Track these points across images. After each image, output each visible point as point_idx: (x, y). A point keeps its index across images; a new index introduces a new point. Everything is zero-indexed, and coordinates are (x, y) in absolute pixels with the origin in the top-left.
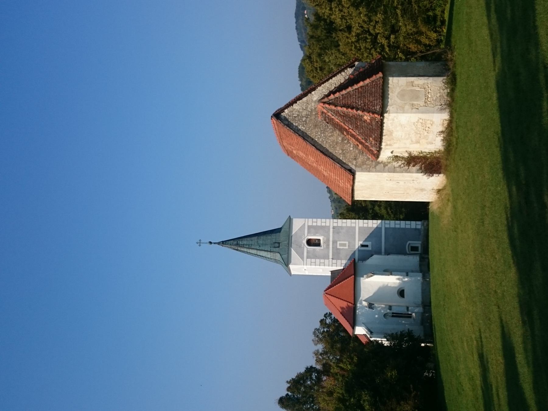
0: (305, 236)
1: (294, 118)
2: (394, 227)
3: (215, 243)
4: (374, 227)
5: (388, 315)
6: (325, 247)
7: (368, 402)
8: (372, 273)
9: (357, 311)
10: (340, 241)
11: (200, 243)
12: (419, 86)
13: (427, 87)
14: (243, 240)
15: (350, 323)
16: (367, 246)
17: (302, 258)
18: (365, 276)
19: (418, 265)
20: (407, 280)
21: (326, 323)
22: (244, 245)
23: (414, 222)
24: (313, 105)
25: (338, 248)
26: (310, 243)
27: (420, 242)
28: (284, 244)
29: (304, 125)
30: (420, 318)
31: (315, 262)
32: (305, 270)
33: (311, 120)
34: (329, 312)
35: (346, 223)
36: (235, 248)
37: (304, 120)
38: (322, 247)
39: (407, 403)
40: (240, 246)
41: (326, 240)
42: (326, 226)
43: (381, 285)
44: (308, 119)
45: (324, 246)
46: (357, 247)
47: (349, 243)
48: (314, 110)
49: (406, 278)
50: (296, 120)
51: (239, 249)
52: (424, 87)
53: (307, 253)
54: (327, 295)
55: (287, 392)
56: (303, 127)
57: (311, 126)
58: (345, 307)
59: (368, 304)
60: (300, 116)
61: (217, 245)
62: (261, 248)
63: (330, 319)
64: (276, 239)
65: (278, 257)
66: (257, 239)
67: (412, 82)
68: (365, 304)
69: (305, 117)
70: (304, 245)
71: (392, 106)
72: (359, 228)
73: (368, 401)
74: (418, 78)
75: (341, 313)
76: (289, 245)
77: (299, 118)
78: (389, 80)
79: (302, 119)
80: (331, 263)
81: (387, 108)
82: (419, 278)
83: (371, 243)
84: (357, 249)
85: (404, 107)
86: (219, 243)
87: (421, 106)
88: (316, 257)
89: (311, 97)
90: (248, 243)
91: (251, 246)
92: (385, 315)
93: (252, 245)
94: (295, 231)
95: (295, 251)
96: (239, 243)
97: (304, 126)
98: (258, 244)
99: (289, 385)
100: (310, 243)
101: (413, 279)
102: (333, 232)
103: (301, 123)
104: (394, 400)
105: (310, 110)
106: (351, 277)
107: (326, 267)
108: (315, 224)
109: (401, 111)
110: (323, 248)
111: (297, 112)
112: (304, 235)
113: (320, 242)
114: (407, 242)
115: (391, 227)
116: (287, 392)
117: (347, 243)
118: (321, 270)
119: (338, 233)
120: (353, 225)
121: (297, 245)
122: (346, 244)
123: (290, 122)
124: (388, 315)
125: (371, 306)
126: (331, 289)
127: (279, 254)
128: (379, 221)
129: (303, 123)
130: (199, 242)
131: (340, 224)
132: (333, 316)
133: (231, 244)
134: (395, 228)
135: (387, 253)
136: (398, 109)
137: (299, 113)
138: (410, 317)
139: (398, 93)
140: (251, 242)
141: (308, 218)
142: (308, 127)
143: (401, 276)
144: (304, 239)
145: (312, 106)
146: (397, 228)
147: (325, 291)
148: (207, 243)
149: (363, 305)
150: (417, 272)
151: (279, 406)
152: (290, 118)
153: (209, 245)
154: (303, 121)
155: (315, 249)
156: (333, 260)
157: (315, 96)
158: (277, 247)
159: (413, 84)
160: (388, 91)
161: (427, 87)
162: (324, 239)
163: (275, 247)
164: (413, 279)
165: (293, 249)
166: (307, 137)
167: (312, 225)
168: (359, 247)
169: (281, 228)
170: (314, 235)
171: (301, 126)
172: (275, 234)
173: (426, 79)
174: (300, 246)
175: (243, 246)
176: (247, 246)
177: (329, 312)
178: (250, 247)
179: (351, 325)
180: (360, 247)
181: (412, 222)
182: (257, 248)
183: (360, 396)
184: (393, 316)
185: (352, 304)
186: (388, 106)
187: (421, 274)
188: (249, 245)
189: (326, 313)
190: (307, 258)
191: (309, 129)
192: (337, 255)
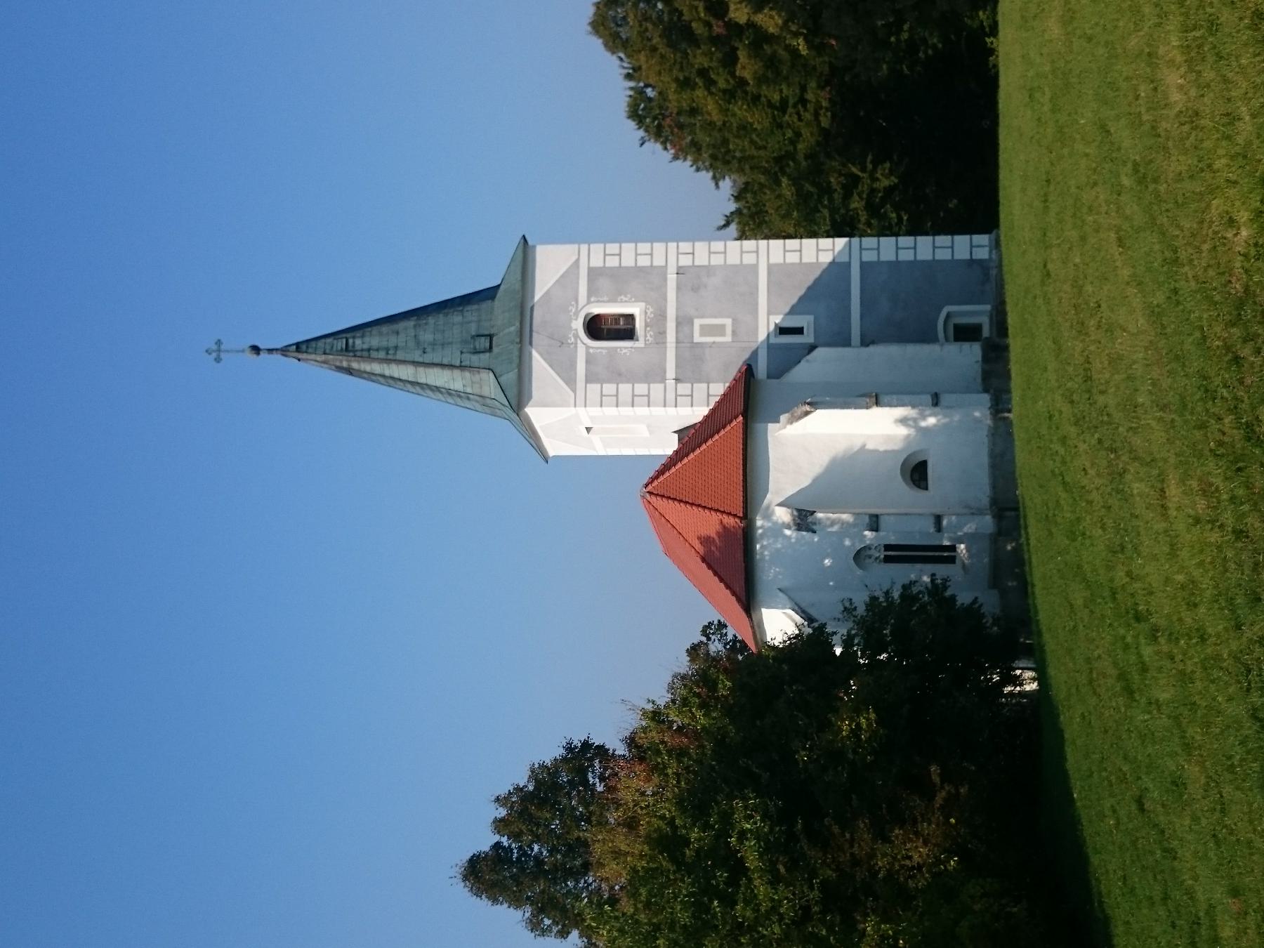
0: (580, 307)
2: (893, 258)
3: (270, 351)
4: (821, 263)
5: (870, 557)
6: (650, 339)
7: (758, 839)
8: (808, 404)
9: (758, 546)
10: (702, 317)
14: (368, 334)
15: (734, 593)
16: (799, 331)
17: (570, 381)
18: (784, 418)
19: (979, 380)
20: (935, 425)
21: (708, 654)
22: (369, 350)
25: (695, 341)
26: (597, 328)
27: (988, 307)
28: (505, 329)
30: (986, 560)
31: (617, 396)
32: (588, 429)
34: (719, 621)
35: (725, 253)
36: (341, 361)
38: (641, 339)
39: (917, 834)
41: (652, 315)
43: (840, 448)
45: (646, 336)
46: (762, 336)
49: (930, 415)
51: (355, 365)
53: (588, 362)
54: (653, 499)
55: (497, 838)
58: (714, 535)
59: (795, 513)
61: (277, 357)
62: (428, 358)
63: (719, 640)
64: (479, 321)
65: (488, 384)
66: (415, 326)
68: (783, 515)
70: (576, 336)
72: (770, 268)
73: (758, 835)
75: (703, 560)
76: (523, 337)
80: (671, 396)
82: (977, 414)
83: (811, 318)
84: (762, 342)
86: (284, 351)
88: (618, 376)
90: (384, 344)
91: (395, 354)
92: (860, 556)
93: (396, 348)
94: (545, 289)
95: (545, 359)
96: (353, 346)
98: (418, 343)
99: (502, 812)
100: (597, 328)
101: (957, 418)
102: (679, 288)
104: (862, 826)
106: (734, 423)
107: (658, 411)
108: (612, 262)
110: (643, 345)
112: (577, 302)
115: (883, 258)
116: (497, 838)
117: (728, 322)
118: (643, 431)
119: (695, 289)
120: (749, 259)
121: (551, 337)
122: (723, 327)
124: (870, 557)
125: (804, 520)
126: (667, 474)
127: (491, 375)
128: (841, 242)
130: (215, 347)
131: (702, 260)
132: (730, 632)
133: (328, 351)
135: (865, 343)
138: (952, 560)
140: (393, 341)
141: (589, 242)
143: (914, 407)
144: (577, 314)
146: (904, 262)
147: (646, 486)
148: (243, 351)
149: (775, 523)
150: (968, 390)
151: (467, 889)
153: (252, 357)
155: (617, 348)
156: (679, 385)
162: (646, 313)
163: (476, 352)
164: (957, 418)
165: (541, 354)
169: (499, 286)
170: (610, 301)
172: (475, 307)
175: (367, 355)
176: (382, 355)
177: (719, 621)
178: (390, 357)
179: (739, 600)
180: (776, 336)
181: (957, 238)
182: (416, 360)
183: (726, 818)
184: (888, 560)
185: (739, 517)
187: (986, 398)
188: (387, 350)
189: (710, 623)
192: (691, 368)
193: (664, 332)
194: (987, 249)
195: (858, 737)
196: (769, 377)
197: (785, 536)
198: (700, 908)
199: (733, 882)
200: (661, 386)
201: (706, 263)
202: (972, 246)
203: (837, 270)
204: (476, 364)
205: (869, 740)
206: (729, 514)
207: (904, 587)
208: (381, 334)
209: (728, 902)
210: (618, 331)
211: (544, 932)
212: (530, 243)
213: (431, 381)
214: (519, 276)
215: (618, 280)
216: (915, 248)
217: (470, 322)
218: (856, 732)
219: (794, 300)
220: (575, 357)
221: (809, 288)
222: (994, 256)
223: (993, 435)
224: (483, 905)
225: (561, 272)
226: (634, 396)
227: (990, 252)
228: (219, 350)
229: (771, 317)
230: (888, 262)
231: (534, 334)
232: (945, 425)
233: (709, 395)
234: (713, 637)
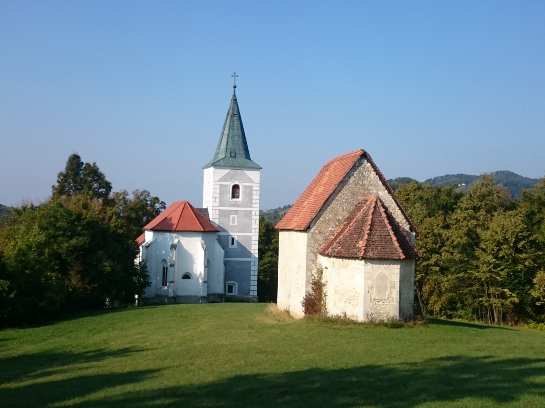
0: (242, 183)
1: (362, 172)
3: (235, 91)
5: (165, 263)
8: (206, 249)
9: (168, 234)
10: (237, 217)
12: (391, 294)
13: (389, 301)
15: (156, 226)
16: (233, 244)
17: (220, 180)
20: (199, 282)
22: (233, 121)
24: (374, 191)
26: (236, 188)
27: (237, 295)
29: (354, 183)
30: (163, 294)
38: (232, 200)
42: (252, 204)
43: (195, 257)
44: (360, 186)
46: (231, 234)
47: (236, 226)
50: (359, 174)
51: (229, 117)
53: (226, 185)
54: (183, 204)
56: (352, 181)
61: (233, 93)
62: (230, 139)
64: (240, 154)
65: (222, 156)
66: (239, 135)
67: (394, 287)
68: (176, 241)
69: (362, 183)
70: (233, 182)
72: (251, 236)
75: (166, 218)
77: (361, 178)
78: (397, 264)
79: (360, 180)
81: (369, 263)
83: (236, 247)
85: (370, 279)
86: (234, 95)
87: (371, 295)
88: (222, 193)
89: (382, 189)
90: (235, 126)
91: (231, 129)
92: (165, 260)
93: (233, 129)
95: (227, 173)
96: (235, 117)
97: (353, 182)
99: (92, 165)
100: (236, 188)
101: (201, 287)
102: (246, 211)
105: (369, 188)
106: (202, 228)
108: (254, 193)
109: (366, 277)
111: (367, 176)
112: (244, 182)
117: (236, 224)
119: (246, 216)
120: (253, 231)
123: (358, 168)
125: (174, 247)
127: (224, 157)
128: (257, 256)
129: (356, 181)
131: (254, 217)
132: (162, 210)
135: (226, 263)
138: (163, 285)
139: (384, 274)
140: (235, 128)
141: (260, 186)
142: (352, 187)
143: (204, 276)
144: (240, 182)
145: (373, 190)
147: (188, 202)
148: (235, 83)
149: (174, 239)
152: (362, 168)
153: (233, 85)
156: (218, 211)
157: (383, 193)
158: (231, 155)
161: (389, 301)
163: (231, 153)
164: (201, 287)
165: (228, 172)
166: (342, 185)
169: (250, 159)
171: (354, 179)
172: (244, 153)
174: (232, 178)
175: (232, 120)
176: (232, 125)
177: (166, 207)
178: (231, 127)
179: (154, 228)
181: (256, 287)
184: (164, 268)
186: (372, 263)
187: (205, 295)
188: (233, 126)
192: (223, 214)
193: (233, 207)
194: (253, 295)
195: (104, 267)
196: (219, 236)
197: (170, 241)
198: (60, 229)
199: (68, 236)
200: (218, 205)
202: (254, 291)
203: (249, 254)
204: (227, 153)
205: (103, 269)
206: (177, 226)
207: (149, 275)
208: (238, 124)
209: (63, 235)
210: (235, 194)
211: (59, 177)
212: (261, 170)
213: (223, 139)
214: (251, 166)
215: (249, 195)
217: (240, 151)
218: (105, 266)
219: (242, 243)
221: (244, 247)
222: (251, 296)
223: (196, 296)
224: (66, 160)
225: (252, 178)
226: (216, 198)
228: (235, 76)
230: (251, 268)
232: (199, 284)
233: (215, 219)
234: (161, 205)
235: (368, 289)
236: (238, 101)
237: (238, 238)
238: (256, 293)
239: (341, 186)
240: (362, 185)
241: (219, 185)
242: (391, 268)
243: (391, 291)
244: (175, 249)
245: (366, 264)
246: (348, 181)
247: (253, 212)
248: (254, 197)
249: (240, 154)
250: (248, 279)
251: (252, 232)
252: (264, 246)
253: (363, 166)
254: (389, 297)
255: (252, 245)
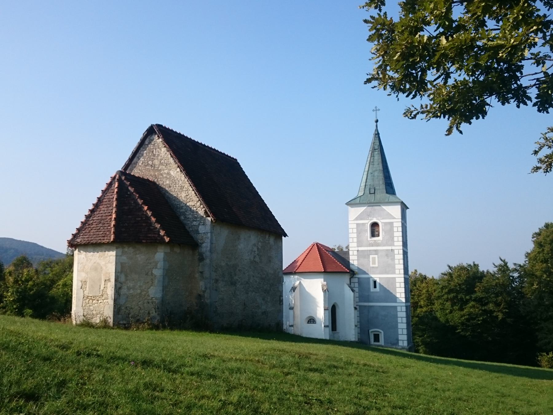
0: (381, 220)
1: (152, 150)
4: (396, 294)
9: (292, 276)
10: (378, 258)
11: (376, 110)
12: (105, 289)
13: (103, 298)
16: (375, 287)
17: (357, 219)
22: (374, 156)
23: (406, 339)
24: (165, 171)
25: (370, 256)
26: (375, 225)
29: (144, 164)
31: (353, 233)
33: (149, 171)
37: (149, 162)
38: (371, 239)
40: (373, 153)
42: (394, 241)
44: (150, 167)
46: (373, 276)
47: (377, 267)
48: (159, 173)
50: (149, 153)
52: (104, 295)
53: (363, 224)
56: (141, 162)
57: (143, 172)
60: (154, 158)
62: (369, 175)
67: (109, 280)
70: (371, 220)
71: (85, 257)
72: (395, 278)
74: (114, 286)
75: (295, 261)
76: (370, 204)
77: (152, 157)
78: (113, 251)
79: (150, 161)
81: (83, 251)
85: (83, 271)
86: (377, 130)
87: (84, 291)
89: (174, 168)
90: (375, 161)
95: (364, 211)
96: (375, 151)
97: (142, 163)
98: (374, 171)
100: (375, 225)
102: (387, 250)
103: (145, 160)
105: (159, 169)
106: (323, 269)
108: (395, 229)
109: (79, 268)
110: (368, 240)
111: (158, 154)
113: (376, 237)
114: (383, 331)
115: (398, 313)
117: (376, 265)
119: (387, 255)
120: (397, 272)
123: (148, 146)
129: (146, 162)
130: (377, 109)
131: (397, 257)
134: (397, 317)
136: (81, 265)
137: (157, 156)
139: (98, 264)
140: (376, 163)
142: (141, 169)
144: (378, 219)
145: (164, 170)
148: (376, 117)
152: (152, 146)
153: (375, 119)
154: (148, 162)
156: (356, 251)
157: (175, 172)
158: (370, 192)
159: (108, 281)
160: (101, 251)
161: (103, 298)
163: (370, 189)
165: (365, 209)
166: (131, 168)
167: (393, 227)
168: (372, 279)
171: (143, 160)
172: (384, 188)
173: (112, 296)
174: (369, 216)
178: (371, 163)
186: (86, 252)
190: (357, 224)
191: (139, 170)
194: (402, 345)
200: (356, 246)
201: (396, 258)
203: (394, 299)
216: (402, 323)
217: (379, 186)
220: (364, 220)
221: (388, 291)
222: (399, 347)
225: (392, 214)
227: (401, 346)
229: (378, 279)
230: (397, 315)
231: (371, 207)
233: (353, 260)
235: (81, 284)
236: (380, 135)
237: (380, 280)
238: (406, 344)
239: (130, 170)
240: (152, 166)
241: (356, 224)
242: (106, 255)
243: (106, 286)
244: (294, 291)
245: (79, 253)
246: (137, 162)
247: (395, 250)
248: (396, 234)
249: (379, 189)
250: (396, 327)
251: (396, 273)
252: (466, 295)
253: (153, 143)
254: (104, 293)
255: (396, 287)
